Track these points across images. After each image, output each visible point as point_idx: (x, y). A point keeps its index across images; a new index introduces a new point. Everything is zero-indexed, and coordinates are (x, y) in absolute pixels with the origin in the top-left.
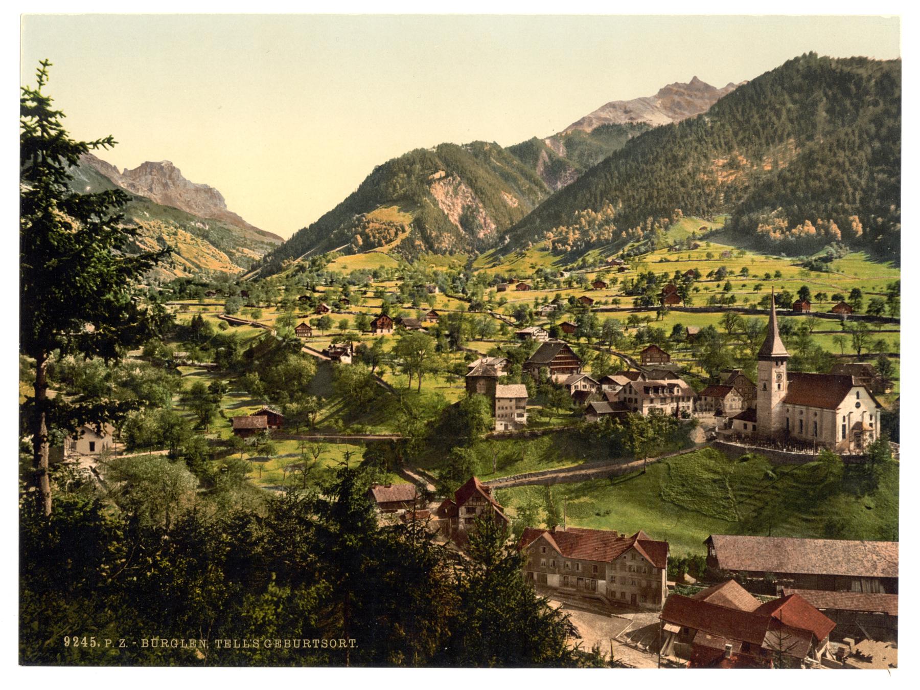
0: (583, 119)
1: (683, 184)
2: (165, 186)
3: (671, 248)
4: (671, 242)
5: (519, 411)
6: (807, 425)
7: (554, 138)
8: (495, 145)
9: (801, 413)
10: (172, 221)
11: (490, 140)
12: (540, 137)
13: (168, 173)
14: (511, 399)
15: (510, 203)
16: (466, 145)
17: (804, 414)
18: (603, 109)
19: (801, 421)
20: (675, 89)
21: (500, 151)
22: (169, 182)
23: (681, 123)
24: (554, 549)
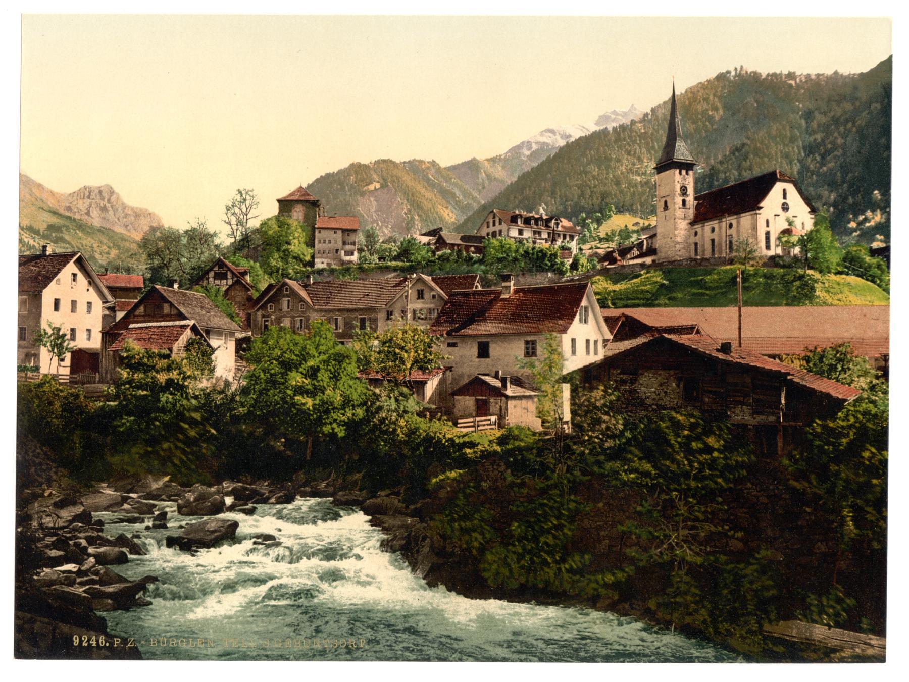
0: (523, 143)
1: (618, 183)
2: (104, 209)
3: (601, 240)
4: (602, 235)
5: (348, 247)
6: (720, 245)
7: (493, 160)
8: (433, 163)
9: (713, 230)
10: (105, 241)
11: (428, 159)
12: (478, 158)
13: (107, 197)
14: (335, 230)
15: (447, 217)
16: (404, 162)
17: (717, 230)
18: (542, 134)
19: (713, 241)
20: (613, 116)
21: (439, 170)
22: (108, 205)
23: (614, 129)
24: (302, 300)
